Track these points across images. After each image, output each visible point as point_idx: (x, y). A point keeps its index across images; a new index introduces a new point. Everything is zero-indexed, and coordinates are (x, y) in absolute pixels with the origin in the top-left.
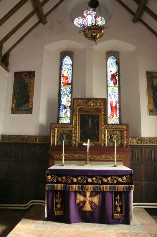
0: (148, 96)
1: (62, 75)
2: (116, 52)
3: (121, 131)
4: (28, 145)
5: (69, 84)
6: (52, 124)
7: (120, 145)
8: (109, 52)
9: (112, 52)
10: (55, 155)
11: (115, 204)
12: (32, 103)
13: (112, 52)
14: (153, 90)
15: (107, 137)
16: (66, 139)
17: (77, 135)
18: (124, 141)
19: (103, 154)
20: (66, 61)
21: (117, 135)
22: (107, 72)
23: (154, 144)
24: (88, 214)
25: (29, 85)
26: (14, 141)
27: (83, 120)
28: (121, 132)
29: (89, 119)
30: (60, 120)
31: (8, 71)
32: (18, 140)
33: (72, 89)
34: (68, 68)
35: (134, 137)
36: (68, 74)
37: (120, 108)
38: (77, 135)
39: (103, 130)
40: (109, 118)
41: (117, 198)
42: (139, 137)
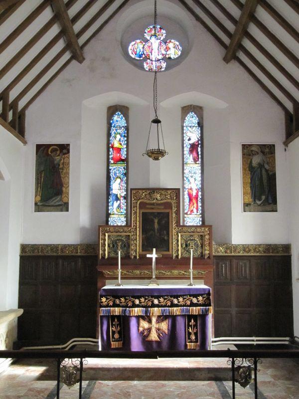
0: (243, 183)
1: (110, 145)
2: (197, 106)
3: (201, 235)
5: (123, 160)
6: (100, 226)
7: (200, 256)
8: (187, 108)
10: (107, 272)
11: (188, 331)
12: (68, 195)
14: (251, 174)
16: (122, 248)
17: (138, 243)
18: (205, 250)
19: (174, 268)
20: (117, 121)
22: (183, 140)
23: (250, 254)
24: (154, 345)
25: (61, 166)
27: (146, 220)
31: (25, 143)
32: (48, 251)
33: (127, 168)
34: (120, 134)
36: (121, 144)
37: (202, 199)
40: (186, 214)
41: (190, 324)
42: (228, 245)
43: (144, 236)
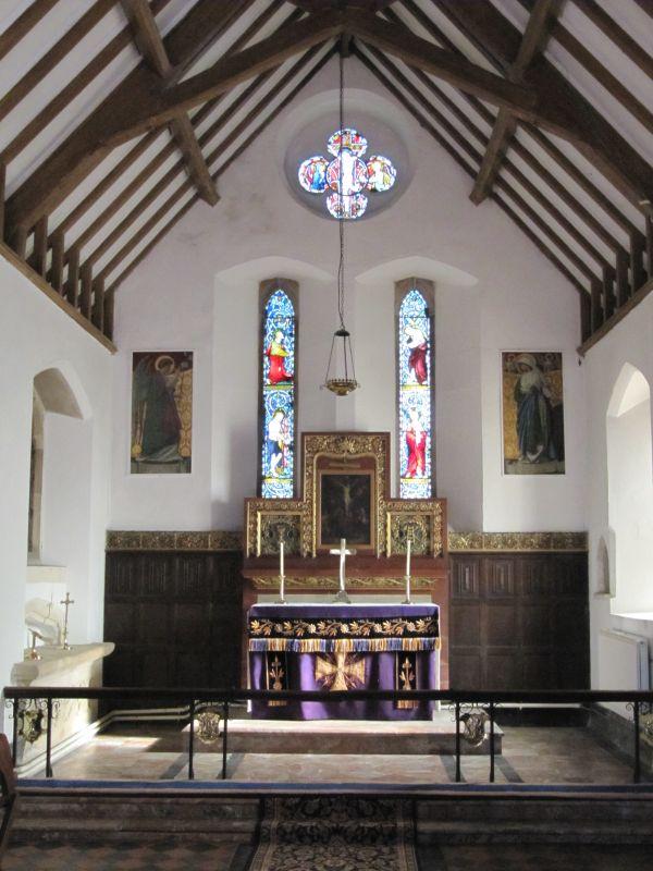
0: (505, 422)
3: (428, 517)
4: (186, 556)
5: (288, 379)
10: (260, 580)
15: (392, 533)
16: (285, 539)
18: (434, 542)
22: (398, 342)
25: (177, 392)
26: (144, 546)
27: (330, 488)
28: (429, 519)
31: (113, 350)
33: (295, 394)
36: (284, 349)
37: (433, 450)
43: (326, 517)
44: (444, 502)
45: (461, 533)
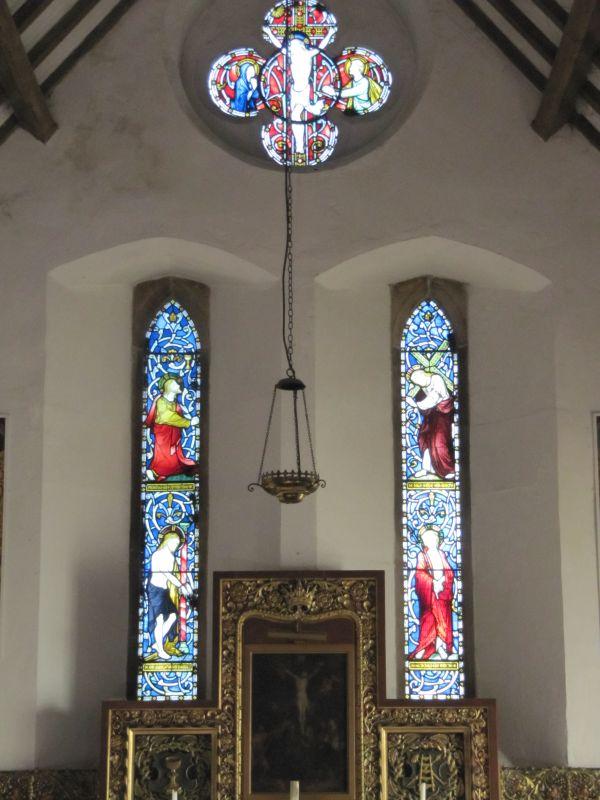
1: (144, 418)
2: (447, 282)
3: (460, 736)
5: (188, 471)
9: (429, 282)
13: (429, 282)
16: (182, 782)
17: (239, 763)
18: (473, 787)
21: (439, 757)
22: (397, 399)
27: (269, 682)
28: (461, 741)
29: (296, 676)
30: (140, 677)
33: (202, 499)
35: (529, 769)
36: (181, 413)
37: (466, 605)
38: (239, 763)
39: (366, 733)
42: (555, 768)
44: (489, 705)
45: (525, 768)
